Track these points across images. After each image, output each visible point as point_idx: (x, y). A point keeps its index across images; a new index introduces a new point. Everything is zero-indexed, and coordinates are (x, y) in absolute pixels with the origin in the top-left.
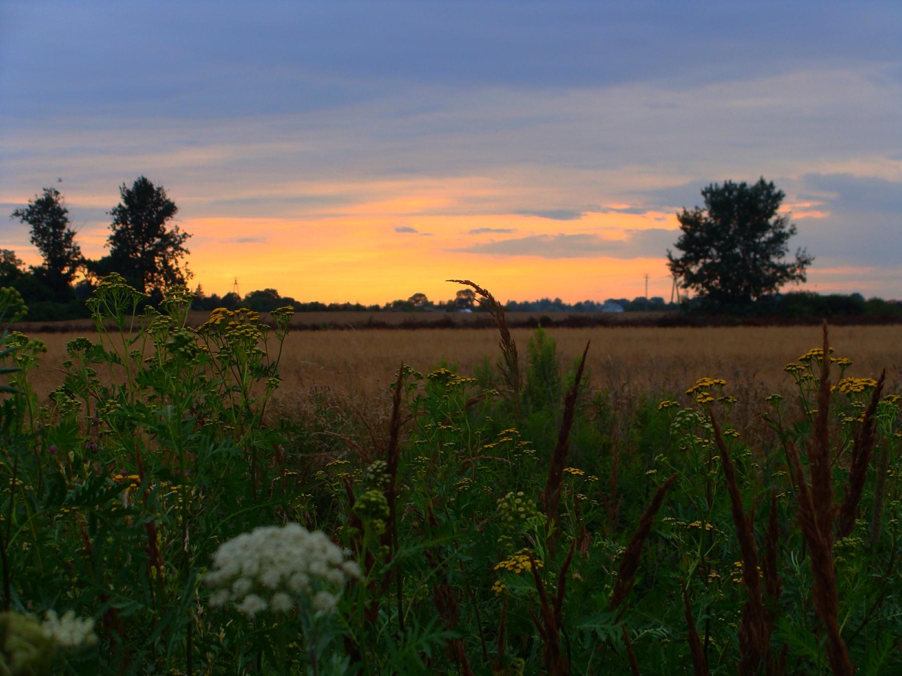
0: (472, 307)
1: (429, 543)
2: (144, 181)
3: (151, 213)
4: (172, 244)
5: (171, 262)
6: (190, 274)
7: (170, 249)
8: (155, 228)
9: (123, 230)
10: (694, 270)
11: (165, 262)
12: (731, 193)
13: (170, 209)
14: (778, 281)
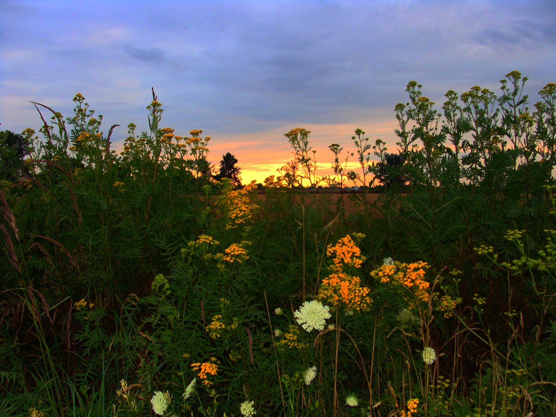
0: (315, 188)
1: (464, 324)
2: (229, 153)
3: (231, 162)
4: (236, 171)
5: (236, 176)
6: (241, 179)
7: (236, 172)
8: (232, 166)
9: (223, 167)
10: (383, 178)
11: (234, 176)
12: (393, 157)
13: (236, 161)
14: (80, 160)
